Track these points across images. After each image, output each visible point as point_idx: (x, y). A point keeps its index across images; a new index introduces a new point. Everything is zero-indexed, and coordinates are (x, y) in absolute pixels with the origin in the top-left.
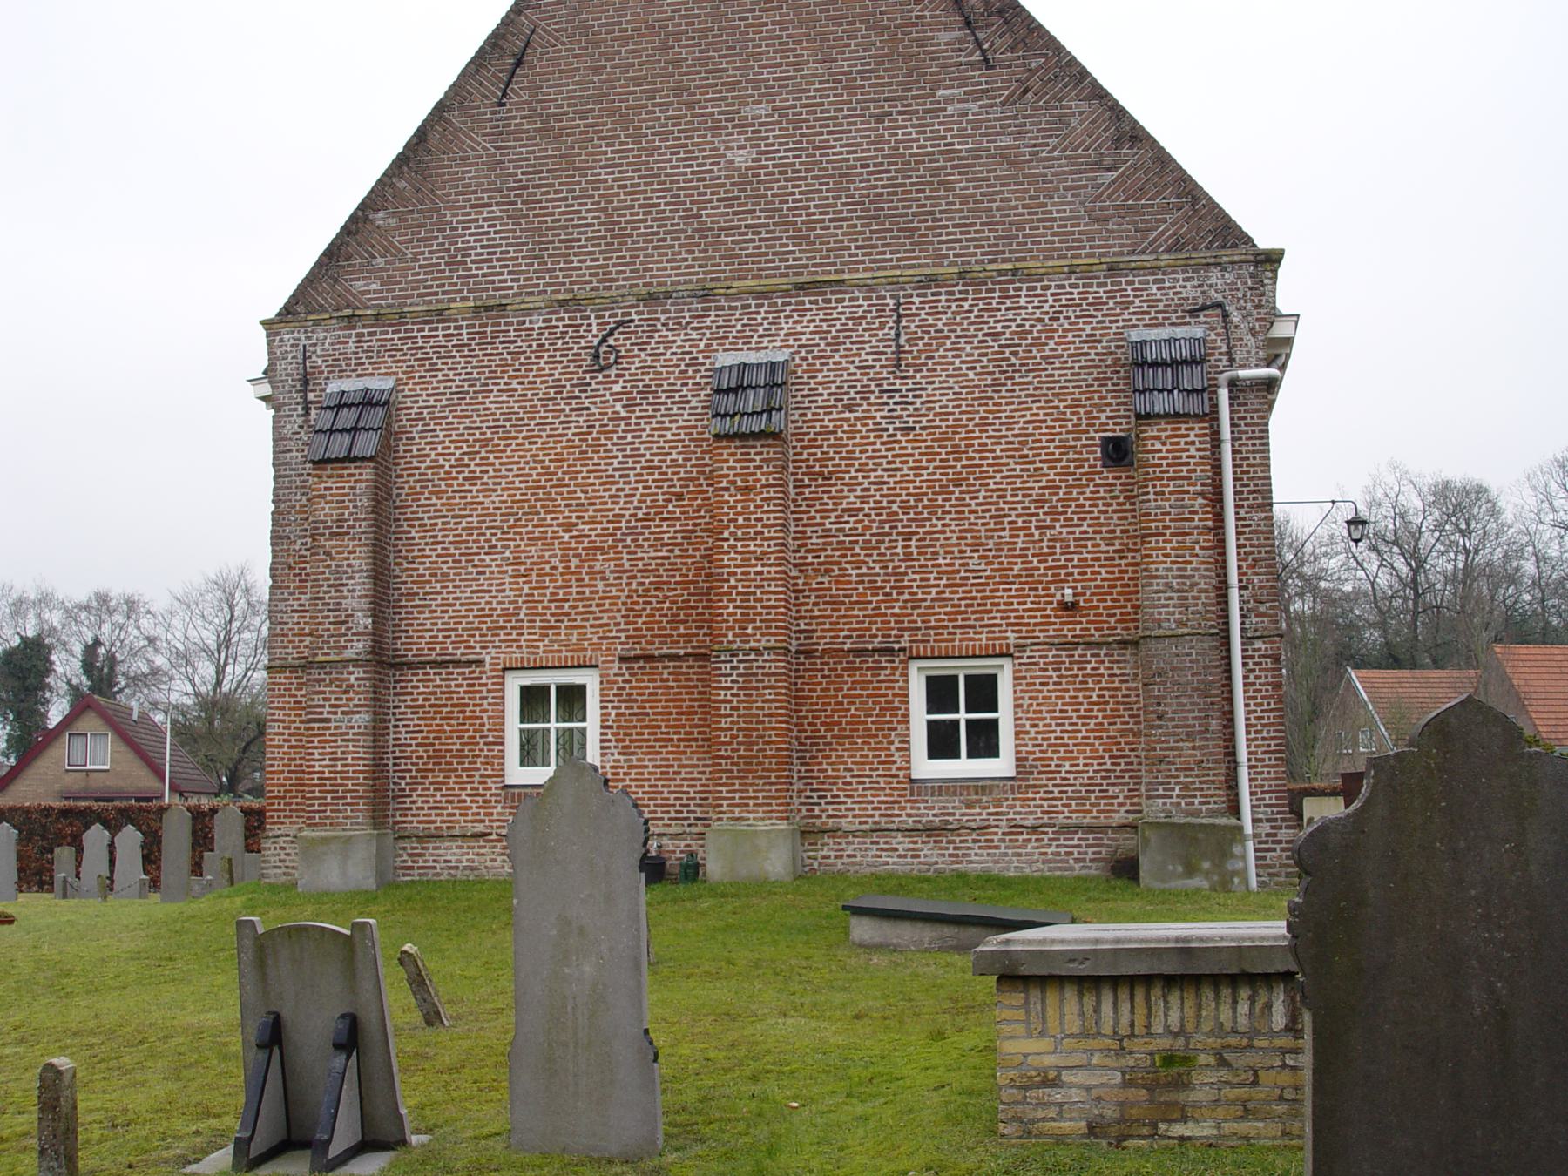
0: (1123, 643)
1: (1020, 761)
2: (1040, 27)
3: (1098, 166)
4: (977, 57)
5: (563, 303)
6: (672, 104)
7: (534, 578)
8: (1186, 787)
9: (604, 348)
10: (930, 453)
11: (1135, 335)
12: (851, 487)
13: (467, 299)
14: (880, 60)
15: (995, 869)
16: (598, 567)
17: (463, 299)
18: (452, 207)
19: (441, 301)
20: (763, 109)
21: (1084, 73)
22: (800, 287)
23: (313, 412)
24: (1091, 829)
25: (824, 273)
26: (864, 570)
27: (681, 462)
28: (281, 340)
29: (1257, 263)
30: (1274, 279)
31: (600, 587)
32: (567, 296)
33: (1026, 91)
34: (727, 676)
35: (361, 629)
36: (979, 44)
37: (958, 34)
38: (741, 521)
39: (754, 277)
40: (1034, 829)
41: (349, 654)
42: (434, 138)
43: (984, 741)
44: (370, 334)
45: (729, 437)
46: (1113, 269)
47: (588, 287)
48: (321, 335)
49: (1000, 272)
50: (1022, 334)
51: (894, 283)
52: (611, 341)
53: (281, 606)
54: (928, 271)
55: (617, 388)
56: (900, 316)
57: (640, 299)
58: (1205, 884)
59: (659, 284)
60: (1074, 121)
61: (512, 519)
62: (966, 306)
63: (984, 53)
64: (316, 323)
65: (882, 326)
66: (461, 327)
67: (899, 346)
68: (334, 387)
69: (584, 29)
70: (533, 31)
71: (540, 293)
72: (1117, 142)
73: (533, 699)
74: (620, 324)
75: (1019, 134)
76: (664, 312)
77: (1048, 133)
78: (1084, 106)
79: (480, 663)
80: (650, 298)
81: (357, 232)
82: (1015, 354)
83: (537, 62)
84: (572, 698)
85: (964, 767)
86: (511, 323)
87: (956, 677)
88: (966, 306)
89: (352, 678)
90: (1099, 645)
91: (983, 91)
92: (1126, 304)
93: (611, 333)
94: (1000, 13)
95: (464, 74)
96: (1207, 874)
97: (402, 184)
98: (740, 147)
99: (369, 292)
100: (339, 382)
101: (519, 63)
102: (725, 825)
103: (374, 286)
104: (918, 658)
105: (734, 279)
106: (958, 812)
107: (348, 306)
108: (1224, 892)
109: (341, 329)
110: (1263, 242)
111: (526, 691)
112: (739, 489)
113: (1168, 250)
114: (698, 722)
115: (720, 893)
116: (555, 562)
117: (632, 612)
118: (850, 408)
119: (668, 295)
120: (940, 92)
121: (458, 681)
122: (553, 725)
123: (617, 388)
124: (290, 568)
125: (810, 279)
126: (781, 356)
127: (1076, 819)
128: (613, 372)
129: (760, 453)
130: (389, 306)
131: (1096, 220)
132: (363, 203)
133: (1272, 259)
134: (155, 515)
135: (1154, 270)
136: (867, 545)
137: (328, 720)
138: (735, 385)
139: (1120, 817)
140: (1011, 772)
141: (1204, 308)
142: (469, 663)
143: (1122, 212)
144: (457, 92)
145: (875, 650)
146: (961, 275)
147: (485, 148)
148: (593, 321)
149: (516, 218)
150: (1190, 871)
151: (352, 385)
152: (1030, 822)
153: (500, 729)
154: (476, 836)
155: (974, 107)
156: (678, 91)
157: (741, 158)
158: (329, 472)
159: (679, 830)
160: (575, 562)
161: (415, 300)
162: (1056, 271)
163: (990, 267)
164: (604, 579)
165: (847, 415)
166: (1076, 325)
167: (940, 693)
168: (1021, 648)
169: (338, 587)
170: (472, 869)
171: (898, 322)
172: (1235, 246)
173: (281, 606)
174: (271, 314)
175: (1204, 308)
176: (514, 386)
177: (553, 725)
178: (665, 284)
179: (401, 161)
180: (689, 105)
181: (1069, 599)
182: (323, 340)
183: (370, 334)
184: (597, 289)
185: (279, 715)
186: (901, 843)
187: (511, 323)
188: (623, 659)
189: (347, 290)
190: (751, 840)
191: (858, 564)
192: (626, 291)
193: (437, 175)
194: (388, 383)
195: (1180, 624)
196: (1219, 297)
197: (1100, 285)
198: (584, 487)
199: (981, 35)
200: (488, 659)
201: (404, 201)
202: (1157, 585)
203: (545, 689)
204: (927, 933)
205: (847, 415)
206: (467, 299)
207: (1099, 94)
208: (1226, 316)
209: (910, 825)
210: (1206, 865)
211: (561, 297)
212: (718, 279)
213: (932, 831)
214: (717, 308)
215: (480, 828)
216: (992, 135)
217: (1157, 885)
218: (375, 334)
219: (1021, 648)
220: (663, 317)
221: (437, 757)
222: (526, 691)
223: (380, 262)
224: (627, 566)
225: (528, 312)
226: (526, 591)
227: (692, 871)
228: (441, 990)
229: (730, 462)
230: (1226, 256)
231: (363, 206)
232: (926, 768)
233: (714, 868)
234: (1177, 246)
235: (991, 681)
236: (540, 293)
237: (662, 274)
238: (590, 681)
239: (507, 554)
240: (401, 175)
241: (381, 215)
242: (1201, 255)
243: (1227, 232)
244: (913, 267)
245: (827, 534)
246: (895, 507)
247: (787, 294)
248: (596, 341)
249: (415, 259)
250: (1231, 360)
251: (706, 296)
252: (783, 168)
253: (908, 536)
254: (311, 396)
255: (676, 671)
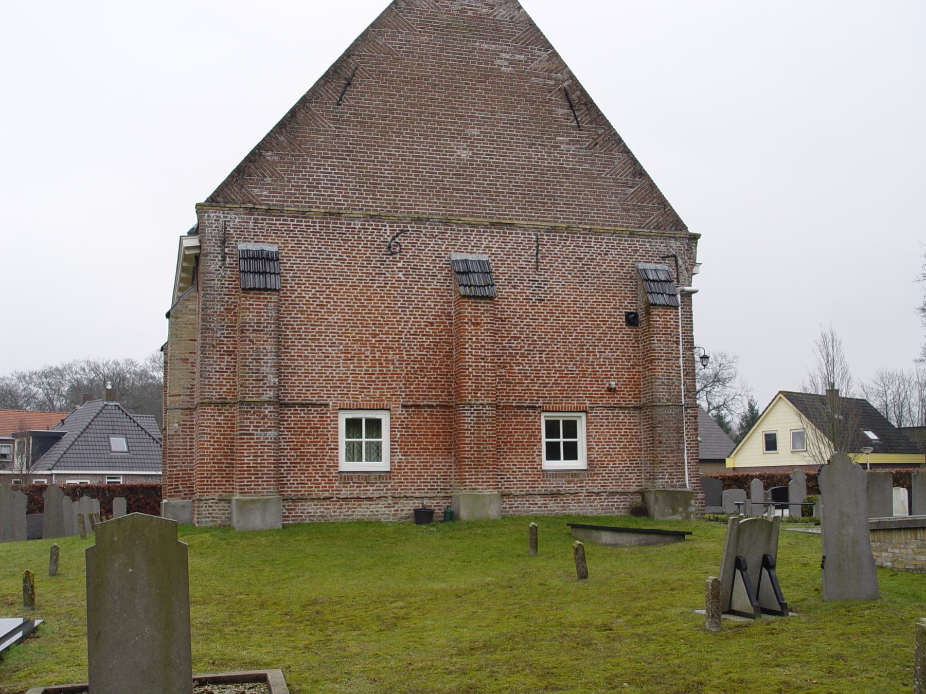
0: (635, 408)
1: (590, 462)
2: (602, 115)
3: (626, 184)
4: (574, 124)
5: (372, 216)
6: (430, 121)
7: (356, 361)
8: (670, 475)
9: (393, 243)
10: (551, 313)
11: (641, 266)
12: (516, 326)
13: (319, 207)
14: (532, 117)
15: (581, 512)
16: (390, 358)
17: (316, 207)
18: (311, 156)
19: (305, 207)
20: (475, 132)
21: (620, 140)
22: (492, 224)
23: (228, 259)
24: (622, 494)
25: (504, 219)
26: (521, 367)
27: (433, 307)
28: (209, 216)
29: (689, 239)
30: (696, 246)
31: (391, 368)
32: (376, 213)
33: (596, 144)
34: (468, 418)
35: (272, 384)
36: (576, 118)
37: (566, 111)
38: (474, 339)
39: (470, 216)
40: (598, 494)
42: (300, 116)
43: (571, 453)
44: (262, 219)
45: (469, 297)
46: (632, 234)
47: (385, 210)
48: (233, 216)
49: (584, 229)
50: (592, 260)
51: (537, 229)
52: (397, 240)
53: (209, 368)
54: (553, 224)
55: (400, 265)
56: (538, 245)
57: (413, 220)
58: (680, 518)
59: (423, 213)
60: (616, 162)
61: (344, 329)
62: (568, 243)
63: (578, 122)
64: (231, 209)
65: (530, 248)
66: (315, 222)
67: (537, 259)
68: (242, 246)
69: (385, 73)
70: (356, 68)
71: (359, 210)
72: (634, 175)
73: (353, 426)
74: (402, 231)
76: (425, 228)
77: (605, 165)
78: (621, 155)
79: (327, 405)
81: (255, 161)
82: (589, 269)
83: (359, 85)
84: (374, 426)
85: (364, 466)
86: (343, 224)
87: (558, 421)
88: (568, 243)
89: (267, 411)
90: (625, 408)
91: (578, 141)
92: (636, 251)
93: (398, 235)
94: (585, 105)
95: (317, 83)
96: (681, 513)
97: (282, 138)
98: (464, 149)
99: (262, 196)
100: (245, 244)
102: (468, 492)
103: (265, 193)
104: (546, 411)
105: (460, 216)
106: (565, 488)
107: (250, 202)
109: (245, 214)
110: (692, 230)
111: (348, 421)
112: (473, 324)
113: (654, 228)
114: (450, 442)
115: (472, 525)
116: (368, 353)
117: (408, 382)
118: (514, 287)
119: (428, 220)
120: (558, 138)
121: (314, 415)
122: (364, 440)
123: (400, 265)
124: (214, 347)
125: (498, 221)
126: (485, 258)
127: (615, 489)
128: (398, 256)
129: (483, 306)
130: (274, 205)
131: (624, 210)
132: (259, 145)
133: (695, 237)
134: (110, 307)
137: (253, 434)
138: (463, 271)
139: (633, 488)
141: (668, 257)
142: (321, 405)
143: (637, 208)
144: (314, 91)
145: (527, 407)
146: (567, 228)
147: (329, 127)
148: (388, 228)
149: (346, 167)
150: (675, 512)
151: (252, 247)
152: (596, 491)
153: (336, 441)
154: (325, 499)
155: (573, 148)
156: (434, 114)
157: (465, 155)
158: (252, 295)
159: (432, 495)
160: (378, 354)
161: (289, 204)
162: (608, 231)
164: (393, 364)
165: (513, 290)
166: (613, 256)
167: (552, 429)
168: (592, 408)
169: (258, 360)
170: (323, 517)
171: (537, 247)
172: (680, 230)
173: (209, 368)
174: (202, 200)
175: (668, 257)
176: (345, 257)
177: (364, 440)
178: (425, 214)
179: (281, 125)
180: (439, 123)
181: (613, 386)
182: (235, 219)
183: (262, 219)
184: (390, 211)
186: (539, 500)
187: (343, 224)
188: (404, 406)
189: (248, 192)
190: (479, 499)
191: (518, 364)
192: (405, 215)
193: (302, 137)
194: (274, 248)
195: (668, 400)
196: (674, 252)
197: (626, 241)
198: (382, 315)
199: (577, 114)
200: (331, 403)
202: (659, 382)
203: (359, 421)
204: (633, 538)
205: (513, 290)
206: (319, 207)
207: (627, 151)
208: (676, 261)
209: (543, 492)
210: (681, 509)
211: (372, 213)
212: (452, 215)
213: (554, 495)
214: (452, 230)
215: (327, 494)
216: (581, 163)
217: (662, 518)
218: (265, 219)
219: (592, 408)
220: (424, 231)
221: (303, 455)
222: (348, 421)
223: (268, 180)
224: (405, 358)
225: (353, 219)
226: (352, 368)
227: (450, 516)
228: (591, 566)
229: (468, 309)
230: (679, 234)
231: (259, 147)
232: (345, 466)
233: (464, 514)
234: (657, 227)
235: (574, 423)
236: (359, 210)
238: (385, 418)
239: (341, 347)
240: (281, 134)
241: (269, 153)
242: (668, 232)
243: (678, 224)
244: (545, 221)
245: (504, 348)
246: (535, 338)
247: (486, 227)
248: (389, 239)
249: (289, 181)
250: (678, 281)
251: (447, 222)
252: (485, 163)
253: (541, 352)
254: (227, 250)
255: (439, 416)
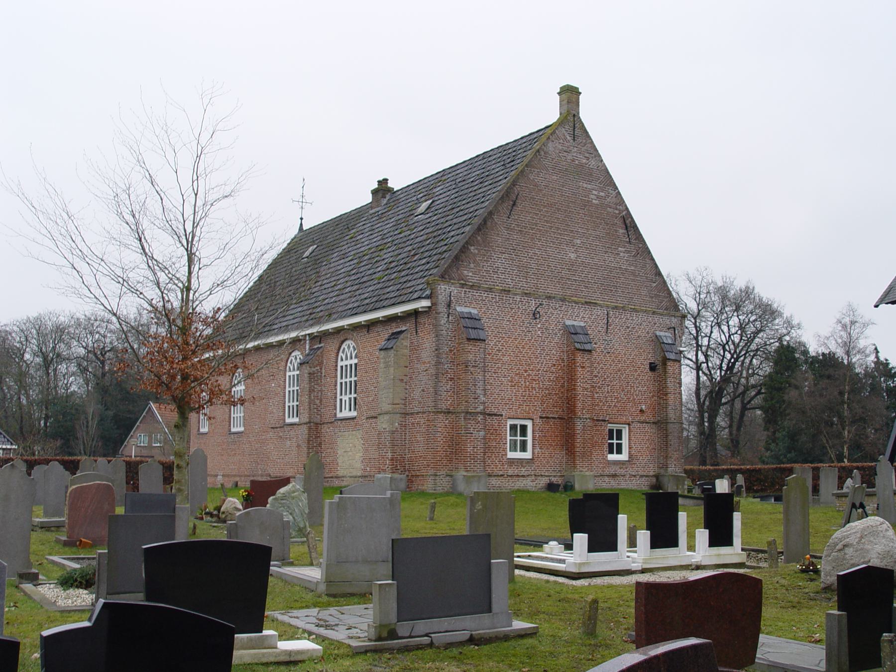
1: (630, 456)
20: (579, 241)
22: (586, 302)
41: (478, 410)
51: (608, 307)
75: (636, 267)
80: (549, 298)
101: (514, 205)
108: (61, 515)
135: (662, 315)
136: (599, 387)
140: (530, 457)
153: (534, 439)
154: (502, 475)
157: (573, 256)
163: (409, 232)
185: (440, 430)
188: (541, 417)
201: (480, 245)
207: (653, 259)
213: (614, 476)
215: (501, 473)
223: (472, 265)
225: (516, 294)
237: (551, 291)
238: (529, 424)
